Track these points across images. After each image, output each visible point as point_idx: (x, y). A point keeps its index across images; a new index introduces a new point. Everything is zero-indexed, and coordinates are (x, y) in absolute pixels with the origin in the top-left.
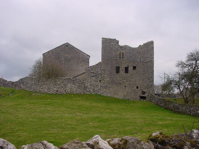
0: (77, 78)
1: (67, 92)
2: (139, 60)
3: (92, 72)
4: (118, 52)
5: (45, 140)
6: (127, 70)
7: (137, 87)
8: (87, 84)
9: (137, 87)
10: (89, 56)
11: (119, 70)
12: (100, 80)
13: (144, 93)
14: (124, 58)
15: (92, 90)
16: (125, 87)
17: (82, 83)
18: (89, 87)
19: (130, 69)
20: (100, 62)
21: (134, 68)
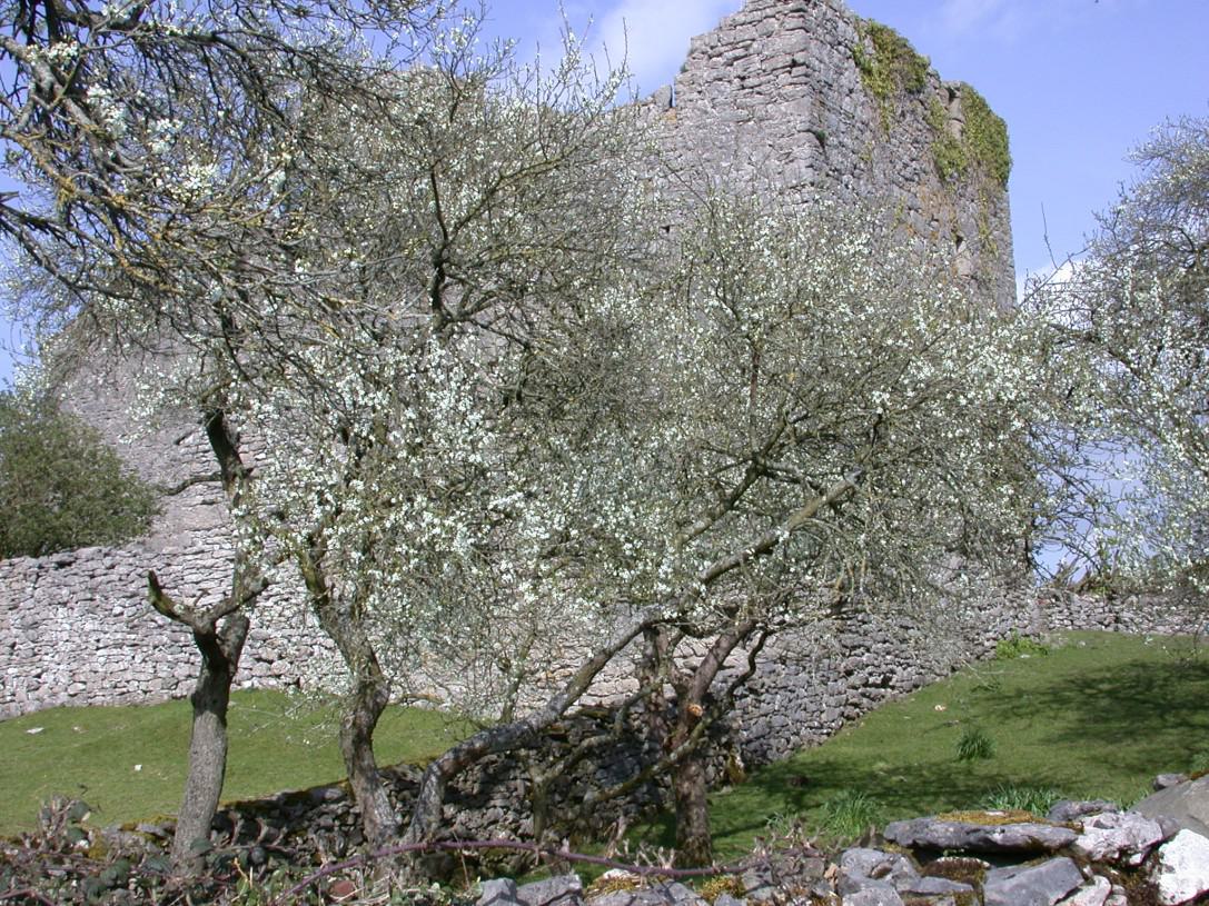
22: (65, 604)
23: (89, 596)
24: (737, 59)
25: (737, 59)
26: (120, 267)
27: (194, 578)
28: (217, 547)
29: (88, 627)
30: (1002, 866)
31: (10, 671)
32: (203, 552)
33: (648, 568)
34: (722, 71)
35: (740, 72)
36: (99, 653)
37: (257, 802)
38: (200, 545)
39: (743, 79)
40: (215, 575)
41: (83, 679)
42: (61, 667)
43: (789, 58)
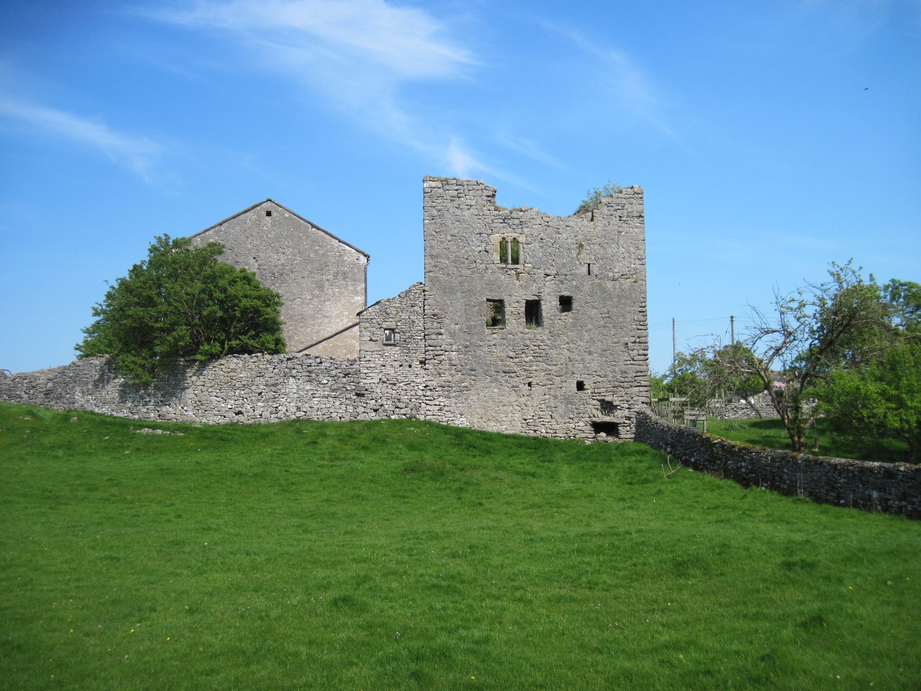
0: (313, 352)
1: (280, 414)
2: (584, 269)
3: (384, 325)
4: (496, 238)
5: (908, 477)
6: (533, 311)
7: (580, 386)
8: (370, 381)
9: (580, 386)
10: (638, 195)
11: (489, 314)
12: (421, 357)
13: (607, 407)
14: (521, 261)
15: (389, 405)
16: (530, 384)
17: (346, 375)
18: (379, 389)
19: (549, 306)
20: (74, 363)
21: (566, 303)
22: (294, 377)
23: (309, 374)
24: (618, 209)
25: (618, 209)
26: (176, 348)
27: (366, 371)
28: (377, 359)
29: (308, 387)
30: (602, 422)
31: (259, 404)
32: (370, 361)
33: (88, 445)
34: (612, 212)
35: (620, 215)
36: (315, 399)
37: (766, 429)
38: (368, 358)
39: (620, 217)
40: (376, 371)
41: (305, 410)
42: (291, 404)
43: (639, 214)
